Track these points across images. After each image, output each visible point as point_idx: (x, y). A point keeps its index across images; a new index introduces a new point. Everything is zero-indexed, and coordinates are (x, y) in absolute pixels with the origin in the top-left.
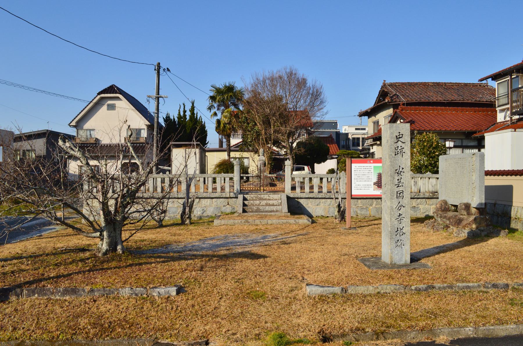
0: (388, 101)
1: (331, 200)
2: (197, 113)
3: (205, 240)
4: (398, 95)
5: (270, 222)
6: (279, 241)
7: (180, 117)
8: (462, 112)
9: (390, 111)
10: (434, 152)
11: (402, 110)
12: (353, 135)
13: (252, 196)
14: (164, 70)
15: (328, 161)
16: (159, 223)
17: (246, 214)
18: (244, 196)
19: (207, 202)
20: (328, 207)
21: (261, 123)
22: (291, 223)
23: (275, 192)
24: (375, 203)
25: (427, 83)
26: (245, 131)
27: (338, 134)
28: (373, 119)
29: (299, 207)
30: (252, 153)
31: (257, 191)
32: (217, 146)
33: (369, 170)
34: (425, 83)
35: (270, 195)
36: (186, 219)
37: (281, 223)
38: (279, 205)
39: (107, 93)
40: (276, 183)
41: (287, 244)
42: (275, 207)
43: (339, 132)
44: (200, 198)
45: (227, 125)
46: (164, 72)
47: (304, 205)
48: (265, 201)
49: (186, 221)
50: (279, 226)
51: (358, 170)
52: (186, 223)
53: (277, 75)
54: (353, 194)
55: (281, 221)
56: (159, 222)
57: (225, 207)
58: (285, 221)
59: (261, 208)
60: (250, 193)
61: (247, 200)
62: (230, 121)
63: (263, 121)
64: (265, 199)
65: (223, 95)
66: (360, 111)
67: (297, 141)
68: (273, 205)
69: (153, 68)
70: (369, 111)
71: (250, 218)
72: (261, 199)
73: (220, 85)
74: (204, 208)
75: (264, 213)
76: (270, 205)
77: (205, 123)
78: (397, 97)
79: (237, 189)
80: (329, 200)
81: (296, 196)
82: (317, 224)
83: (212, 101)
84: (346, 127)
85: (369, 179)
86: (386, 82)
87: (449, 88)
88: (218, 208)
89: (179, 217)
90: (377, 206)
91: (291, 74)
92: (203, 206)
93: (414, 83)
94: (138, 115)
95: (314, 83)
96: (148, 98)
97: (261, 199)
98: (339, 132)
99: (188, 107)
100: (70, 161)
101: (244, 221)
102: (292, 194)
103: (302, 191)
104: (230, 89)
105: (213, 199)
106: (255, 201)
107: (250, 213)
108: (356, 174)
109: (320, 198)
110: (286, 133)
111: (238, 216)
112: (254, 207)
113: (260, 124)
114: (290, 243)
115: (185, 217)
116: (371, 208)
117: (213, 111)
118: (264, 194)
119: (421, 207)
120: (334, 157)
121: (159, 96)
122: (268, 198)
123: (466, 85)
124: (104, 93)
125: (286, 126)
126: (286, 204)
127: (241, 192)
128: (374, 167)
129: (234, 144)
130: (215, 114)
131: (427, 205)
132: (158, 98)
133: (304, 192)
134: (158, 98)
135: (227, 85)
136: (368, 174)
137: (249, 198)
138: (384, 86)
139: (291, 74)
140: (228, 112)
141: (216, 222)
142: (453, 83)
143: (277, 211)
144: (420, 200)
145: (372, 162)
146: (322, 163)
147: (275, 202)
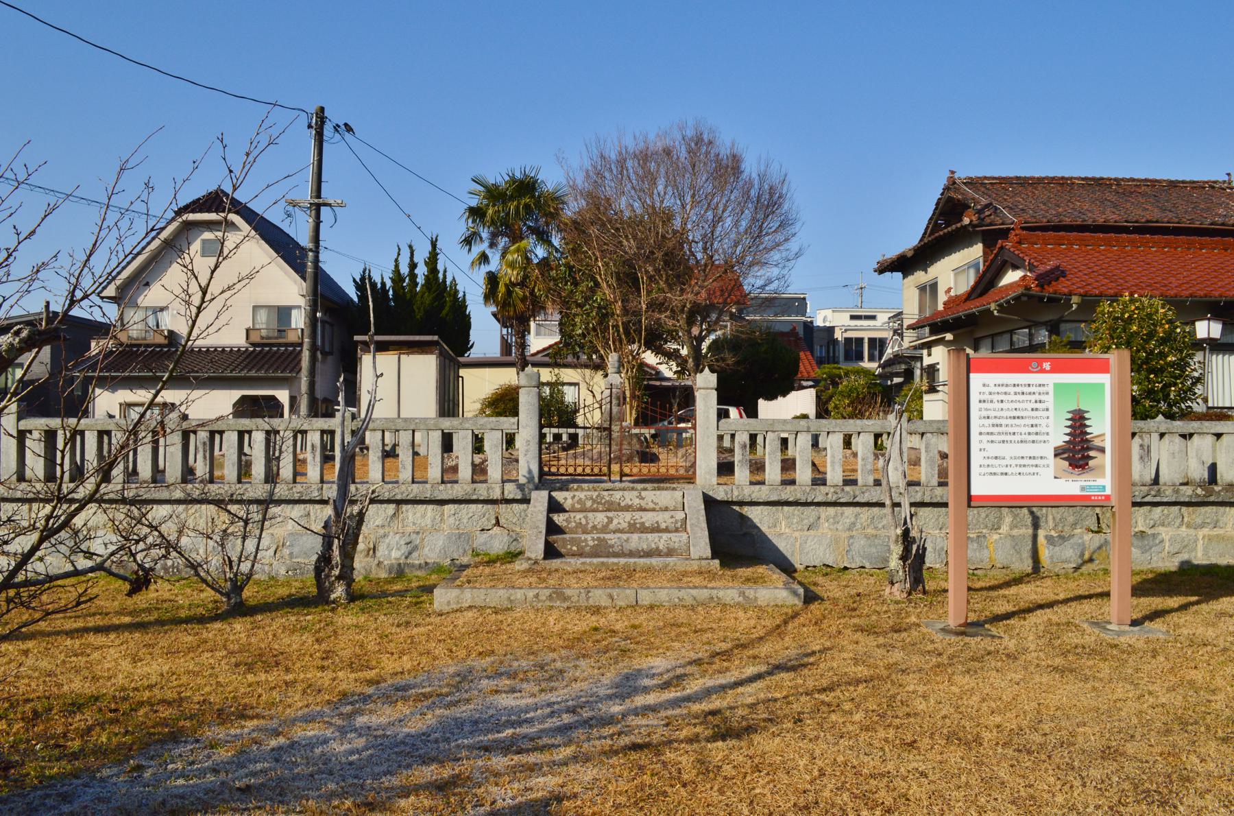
0: (971, 221)
1: (876, 510)
2: (445, 271)
3: (366, 698)
4: (996, 209)
5: (646, 597)
6: (696, 707)
7: (397, 278)
8: (1189, 249)
9: (976, 251)
10: (1163, 355)
11: (1020, 243)
12: (846, 330)
13: (582, 495)
14: (336, 128)
15: (793, 395)
16: (229, 599)
17: (556, 563)
18: (550, 497)
19: (424, 516)
20: (847, 534)
21: (613, 282)
22: (728, 600)
23: (661, 481)
24: (1008, 520)
25: (1067, 179)
26: (565, 304)
27: (809, 327)
28: (920, 277)
29: (745, 534)
30: (587, 372)
31: (597, 478)
32: (495, 351)
33: (1037, 397)
34: (1063, 178)
35: (644, 494)
36: (332, 584)
37: (689, 601)
38: (677, 530)
39: (201, 211)
40: (655, 450)
41: (738, 735)
42: (665, 536)
43: (812, 322)
44: (399, 502)
45: (517, 289)
46: (337, 135)
47: (764, 529)
48: (628, 516)
49: (332, 591)
50: (682, 616)
51: (995, 398)
52: (333, 596)
53: (660, 146)
54: (973, 492)
55: (688, 595)
56: (227, 595)
57: (486, 535)
58: (703, 594)
59: (612, 539)
60: (575, 486)
61: (564, 511)
62: (525, 277)
63: (618, 274)
64: (628, 508)
65: (504, 203)
66: (880, 259)
67: (712, 337)
68: (656, 529)
69: (303, 120)
70: (910, 254)
71: (573, 581)
72: (611, 507)
73: (497, 175)
74: (414, 536)
75: (622, 561)
76: (644, 529)
77: (464, 295)
78: (995, 212)
79: (530, 472)
80: (849, 511)
81: (736, 495)
82: (827, 604)
83: (474, 221)
84: (828, 313)
85: (1036, 433)
86: (956, 176)
87: (1132, 193)
88: (461, 537)
89: (310, 576)
90: (1015, 532)
91: (699, 140)
92: (409, 529)
93: (1032, 178)
94: (282, 268)
95: (763, 168)
96: (290, 208)
97: (611, 507)
98: (812, 322)
99: (421, 256)
100: (98, 391)
101: (547, 592)
102: (721, 488)
103: (724, 479)
104: (525, 187)
105: (446, 507)
106: (590, 515)
107: (572, 561)
108: (985, 413)
109: (819, 504)
110: (682, 311)
111: (529, 571)
112: (589, 537)
113: (609, 286)
114: (750, 730)
115: (328, 576)
116: (996, 537)
117: (477, 249)
118: (624, 489)
119: (1165, 533)
120: (805, 383)
121: (321, 201)
122: (637, 502)
123: (1173, 184)
124: (193, 211)
125: (682, 291)
126: (704, 525)
127: (545, 479)
128: (1056, 385)
129: (540, 348)
130: (484, 258)
131: (1184, 528)
132: (317, 208)
133: (762, 483)
134: (317, 208)
135: (518, 175)
136: (1035, 414)
137: (569, 502)
138: (952, 185)
139: (698, 143)
140: (518, 250)
141: (443, 597)
142: (1138, 180)
143: (670, 553)
144: (1160, 509)
145: (1047, 366)
146: (780, 399)
147: (663, 519)
